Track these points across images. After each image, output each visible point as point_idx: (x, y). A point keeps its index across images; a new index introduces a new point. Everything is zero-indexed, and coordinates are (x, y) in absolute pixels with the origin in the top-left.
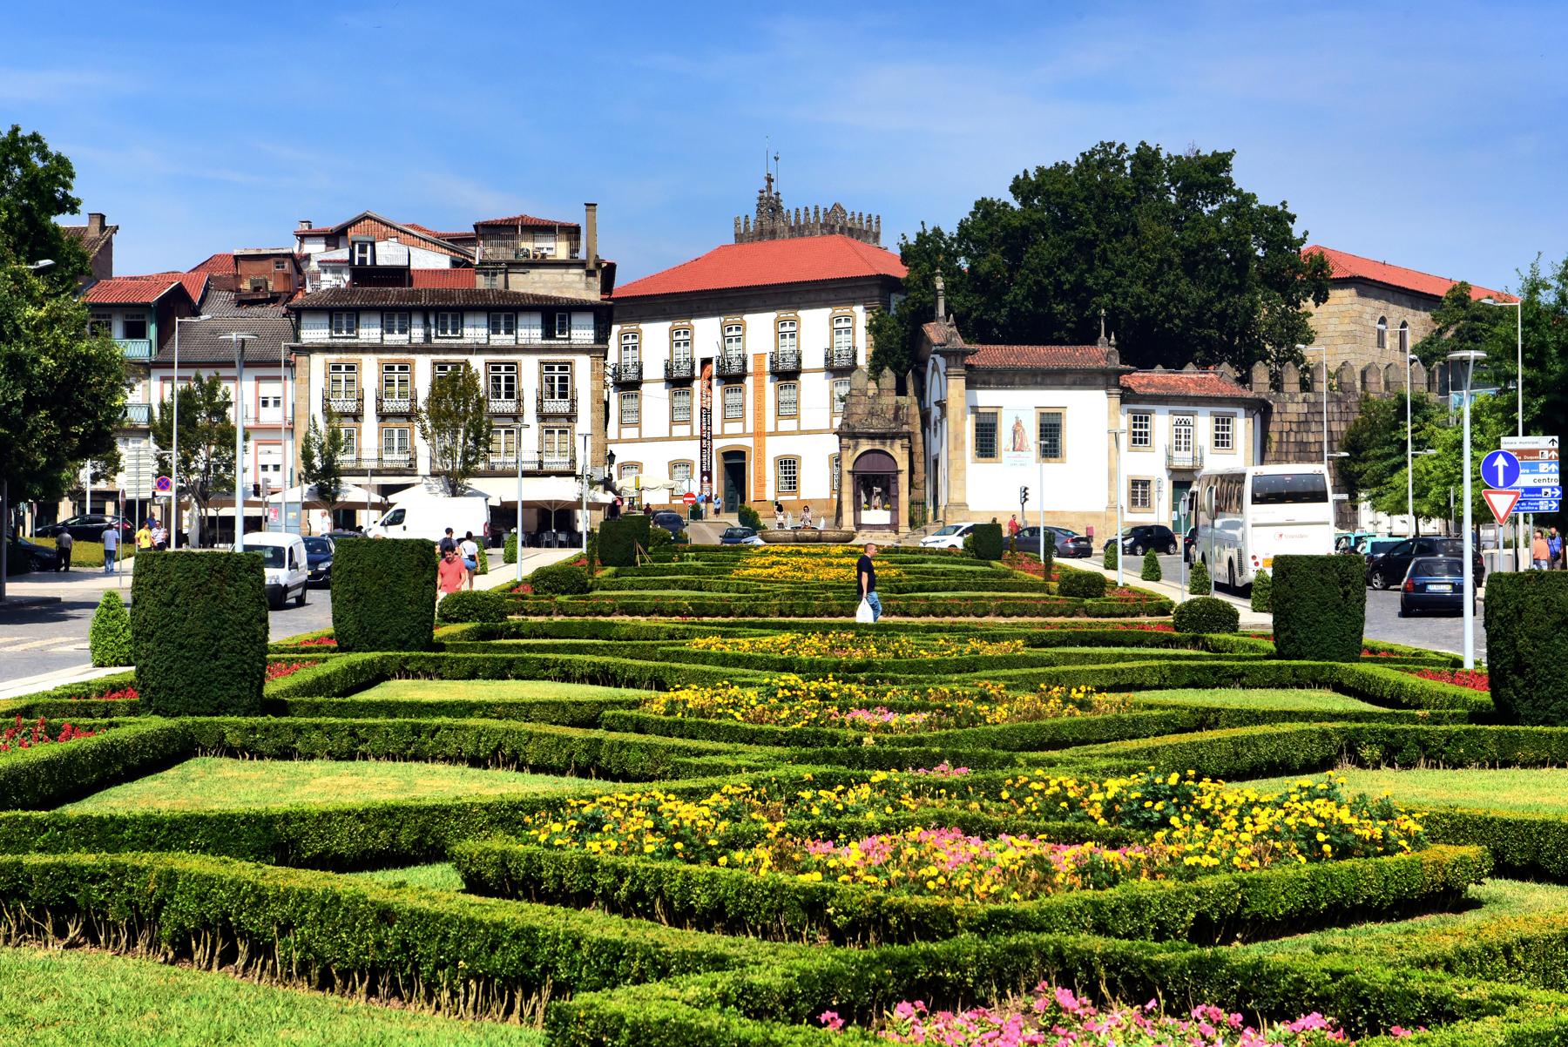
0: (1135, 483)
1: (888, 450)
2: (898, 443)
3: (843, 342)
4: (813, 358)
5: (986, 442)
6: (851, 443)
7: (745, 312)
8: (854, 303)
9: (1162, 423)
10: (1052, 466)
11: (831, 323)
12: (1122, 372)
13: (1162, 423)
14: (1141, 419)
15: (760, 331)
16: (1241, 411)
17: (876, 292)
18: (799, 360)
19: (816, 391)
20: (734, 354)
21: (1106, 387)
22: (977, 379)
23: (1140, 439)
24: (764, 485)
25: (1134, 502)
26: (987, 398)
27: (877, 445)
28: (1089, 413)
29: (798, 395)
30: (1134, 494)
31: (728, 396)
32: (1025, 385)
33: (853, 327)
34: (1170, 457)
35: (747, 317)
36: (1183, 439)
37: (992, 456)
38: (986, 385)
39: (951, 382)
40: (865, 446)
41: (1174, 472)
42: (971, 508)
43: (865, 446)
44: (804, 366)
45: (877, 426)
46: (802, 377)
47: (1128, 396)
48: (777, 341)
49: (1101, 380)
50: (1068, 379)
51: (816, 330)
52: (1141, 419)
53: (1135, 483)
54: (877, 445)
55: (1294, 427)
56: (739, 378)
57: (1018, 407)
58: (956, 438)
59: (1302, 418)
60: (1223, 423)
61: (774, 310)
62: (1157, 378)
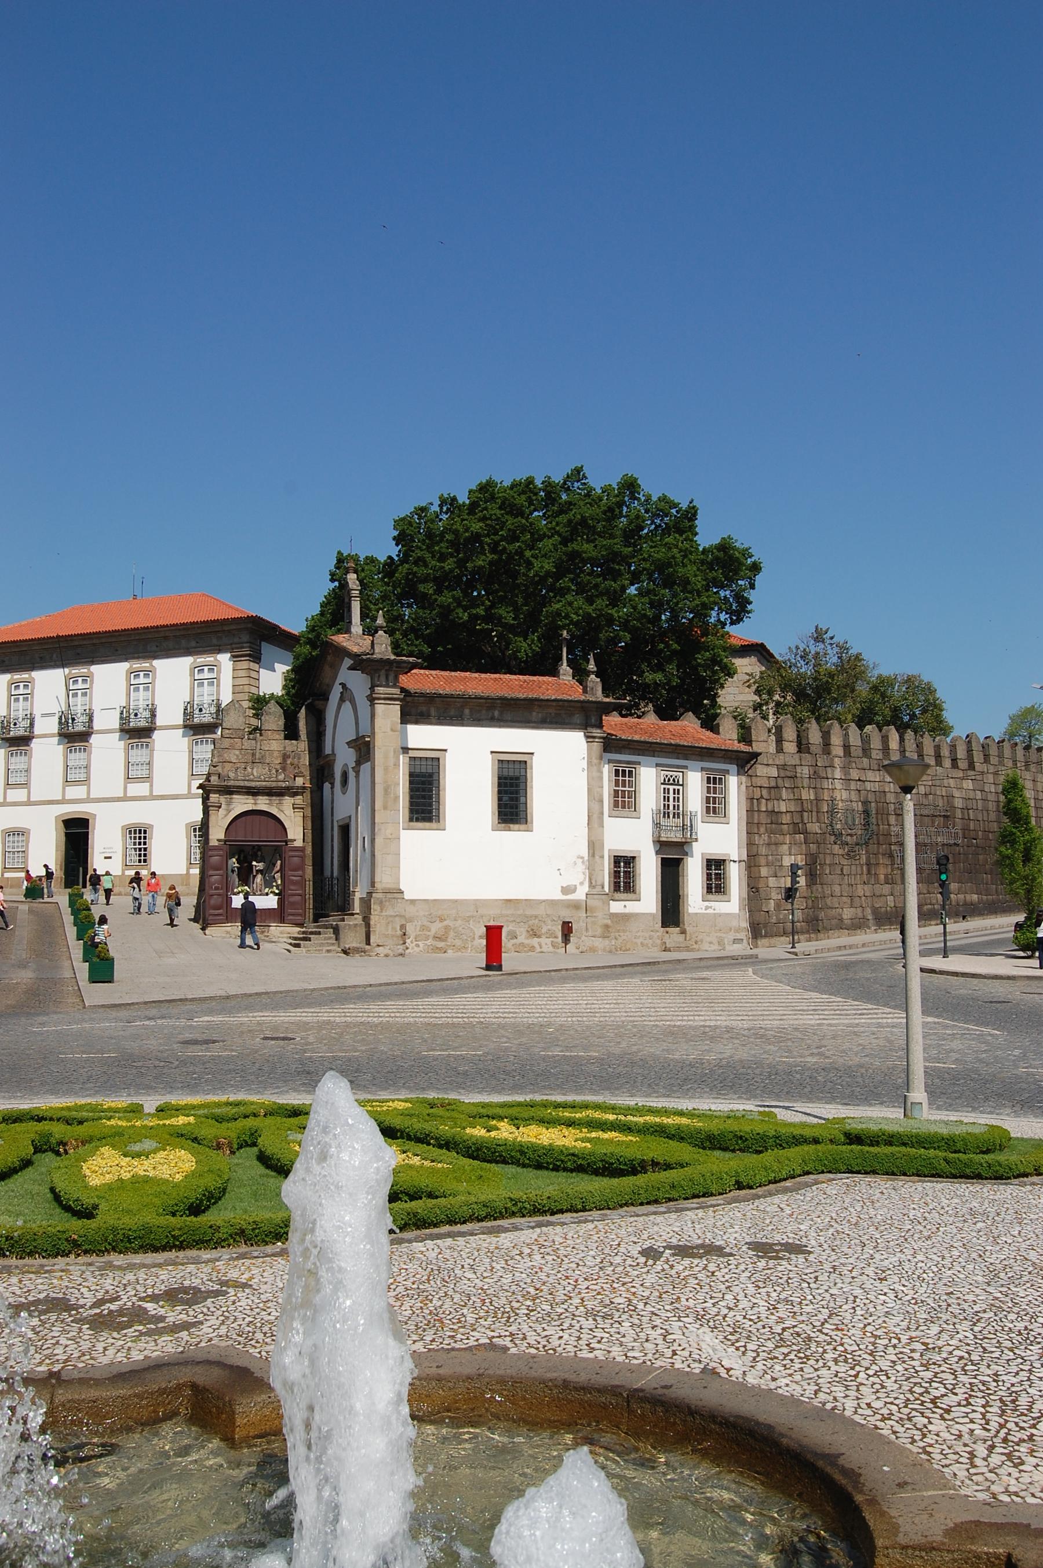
0: (617, 860)
1: (274, 811)
2: (288, 801)
3: (205, 696)
4: (170, 714)
5: (424, 801)
6: (223, 799)
7: (93, 663)
8: (219, 651)
9: (648, 778)
10: (513, 837)
11: (192, 674)
12: (606, 709)
13: (648, 778)
14: (624, 776)
15: (109, 683)
16: (733, 768)
17: (245, 637)
18: (153, 715)
19: (174, 757)
20: (79, 709)
21: (584, 726)
22: (418, 709)
23: (624, 800)
24: (107, 855)
25: (616, 887)
26: (423, 736)
27: (263, 804)
28: (561, 761)
29: (152, 756)
30: (617, 874)
31: (13, 760)
32: (477, 720)
33: (217, 678)
34: (657, 825)
35: (95, 669)
36: (671, 807)
37: (429, 819)
38: (422, 718)
39: (380, 708)
40: (242, 804)
41: (662, 845)
42: (407, 896)
43: (242, 804)
44: (159, 722)
45: (258, 775)
46: (156, 735)
47: (611, 745)
48: (128, 695)
49: (578, 718)
50: (535, 715)
51: (174, 683)
52: (624, 776)
53: (617, 860)
54: (263, 804)
55: (765, 792)
56: (83, 737)
57: (470, 756)
58: (386, 791)
59: (773, 784)
60: (714, 783)
61: (126, 660)
62: (649, 724)
